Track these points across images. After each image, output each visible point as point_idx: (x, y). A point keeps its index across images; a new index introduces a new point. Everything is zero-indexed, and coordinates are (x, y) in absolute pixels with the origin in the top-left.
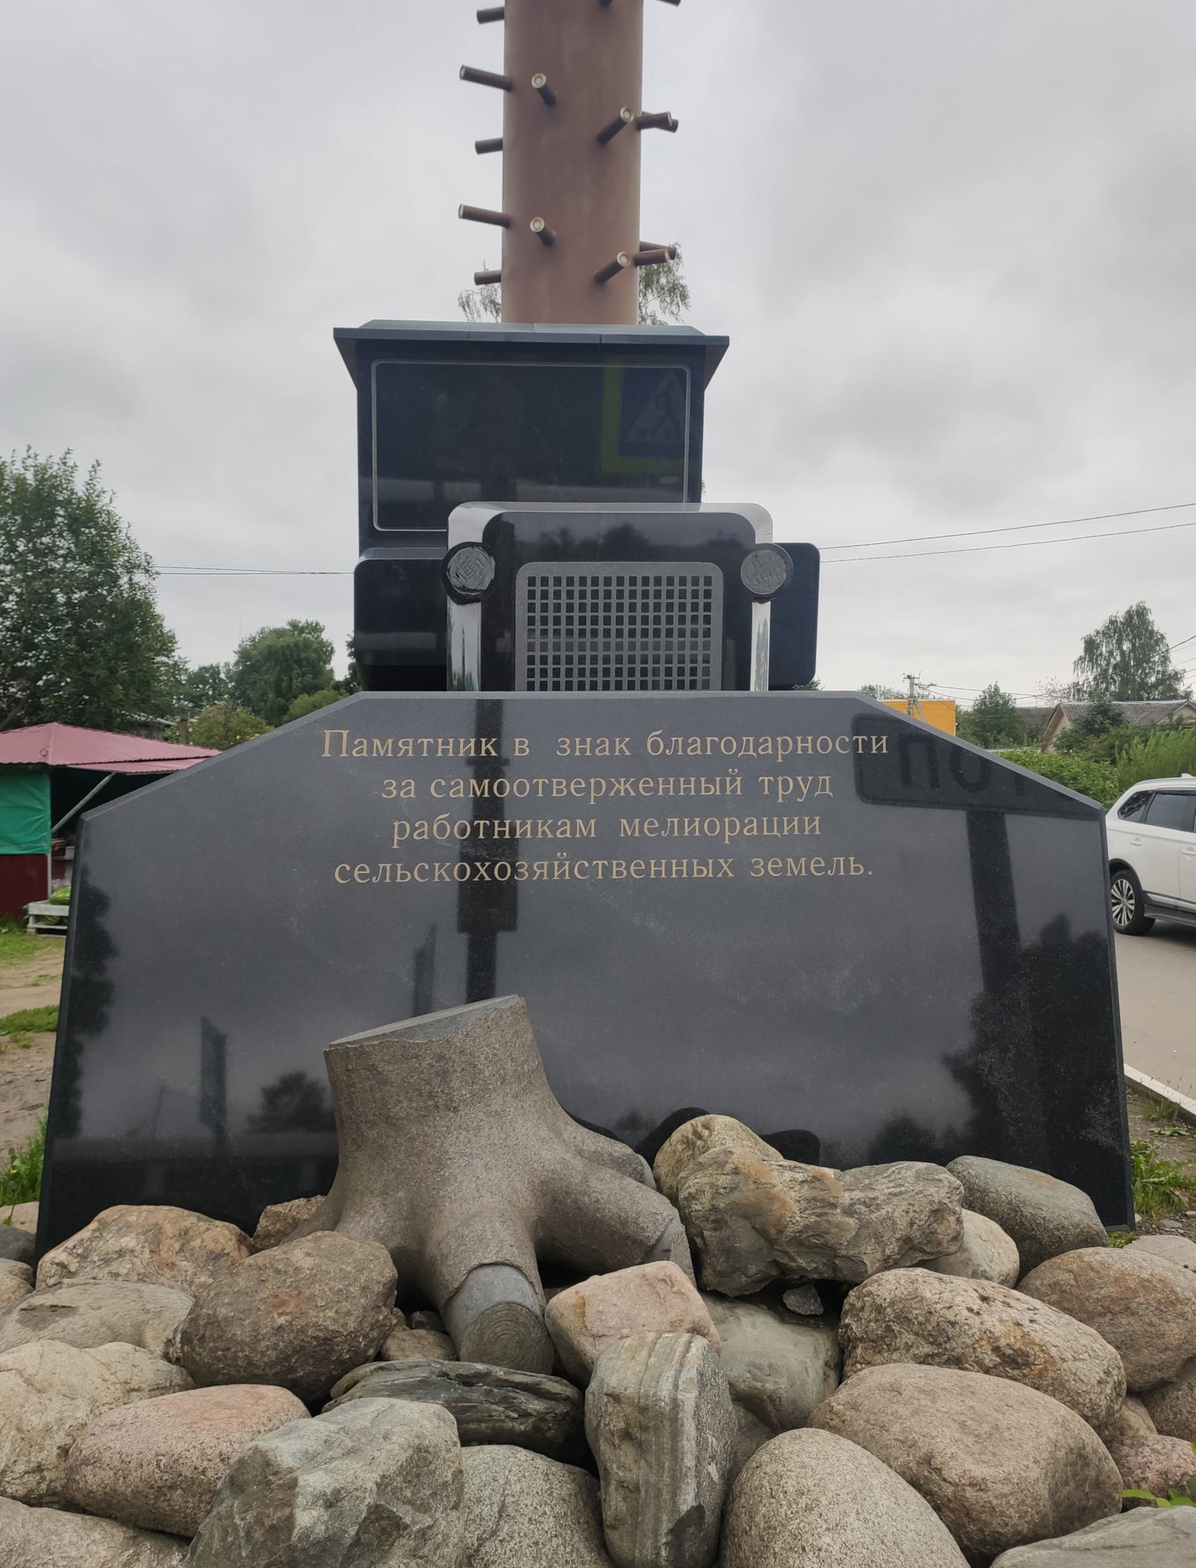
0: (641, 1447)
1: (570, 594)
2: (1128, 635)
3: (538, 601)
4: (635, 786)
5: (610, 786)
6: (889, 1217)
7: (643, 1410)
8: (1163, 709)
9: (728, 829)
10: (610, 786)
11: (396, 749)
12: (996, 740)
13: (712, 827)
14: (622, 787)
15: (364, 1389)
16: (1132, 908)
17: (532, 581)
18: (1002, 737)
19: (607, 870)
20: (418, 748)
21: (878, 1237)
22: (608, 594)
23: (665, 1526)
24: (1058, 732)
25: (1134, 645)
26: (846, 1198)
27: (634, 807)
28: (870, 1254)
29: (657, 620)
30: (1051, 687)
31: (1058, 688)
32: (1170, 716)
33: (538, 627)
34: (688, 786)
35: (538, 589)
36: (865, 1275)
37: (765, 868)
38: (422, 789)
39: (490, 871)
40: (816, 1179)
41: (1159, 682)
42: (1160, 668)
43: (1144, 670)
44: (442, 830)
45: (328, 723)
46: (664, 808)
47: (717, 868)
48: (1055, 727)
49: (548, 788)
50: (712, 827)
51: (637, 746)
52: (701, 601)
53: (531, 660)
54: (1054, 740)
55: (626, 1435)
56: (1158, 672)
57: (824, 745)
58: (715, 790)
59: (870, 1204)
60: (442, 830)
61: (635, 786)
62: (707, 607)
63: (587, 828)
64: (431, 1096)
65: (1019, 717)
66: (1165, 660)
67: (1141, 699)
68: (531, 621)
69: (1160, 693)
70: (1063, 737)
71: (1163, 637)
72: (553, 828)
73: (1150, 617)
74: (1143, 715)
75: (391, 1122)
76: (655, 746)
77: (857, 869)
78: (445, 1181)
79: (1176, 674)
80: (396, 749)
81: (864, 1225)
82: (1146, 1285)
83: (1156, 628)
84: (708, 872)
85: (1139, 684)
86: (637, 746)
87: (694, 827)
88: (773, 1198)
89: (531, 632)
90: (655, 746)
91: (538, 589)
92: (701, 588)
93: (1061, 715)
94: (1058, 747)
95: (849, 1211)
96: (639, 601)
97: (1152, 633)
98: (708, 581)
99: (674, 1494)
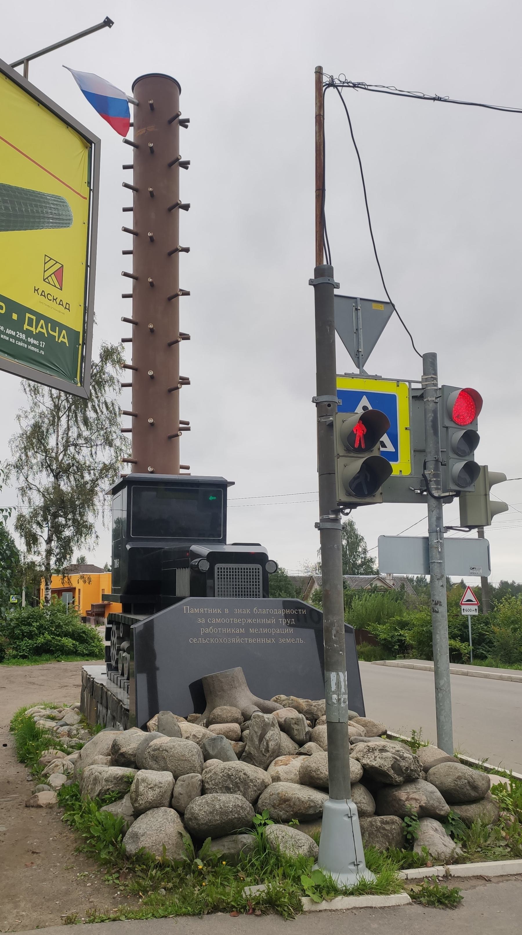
0: (298, 725)
1: (227, 572)
2: (344, 536)
3: (220, 574)
4: (252, 621)
5: (247, 621)
6: (322, 707)
7: (298, 719)
8: (366, 580)
9: (273, 631)
10: (247, 621)
11: (200, 611)
12: (279, 595)
13: (270, 631)
14: (249, 621)
15: (270, 703)
16: (385, 438)
17: (218, 569)
18: (283, 593)
19: (248, 641)
20: (204, 611)
21: (321, 711)
22: (236, 572)
23: (304, 733)
24: (313, 591)
25: (348, 542)
26: (314, 704)
27: (253, 626)
28: (320, 714)
29: (247, 578)
30: (306, 565)
31: (310, 565)
32: (371, 585)
33: (220, 580)
34: (263, 621)
35: (220, 570)
36: (319, 717)
37: (282, 641)
38: (206, 621)
39: (222, 640)
40: (307, 701)
41: (363, 564)
42: (363, 556)
43: (354, 557)
44: (211, 630)
45: (185, 604)
46: (259, 626)
47: (271, 641)
48: (311, 588)
49: (233, 621)
50: (270, 631)
51: (252, 611)
52: (257, 574)
53: (218, 588)
54: (311, 596)
55: (295, 723)
56: (362, 558)
57: (292, 611)
58: (269, 622)
59: (318, 705)
60: (211, 630)
61: (252, 621)
62: (259, 575)
63: (242, 631)
64: (231, 685)
65: (290, 581)
66: (365, 551)
67: (355, 574)
68: (218, 578)
69: (364, 570)
70: (316, 595)
71: (363, 539)
72: (235, 630)
73: (356, 527)
74: (355, 584)
75: (223, 690)
76: (255, 611)
77: (302, 642)
78: (237, 702)
79: (371, 559)
80: (200, 611)
81: (318, 709)
82: (369, 722)
83: (359, 533)
84: (269, 642)
85: (352, 564)
86: (252, 611)
87: (266, 631)
88: (300, 704)
89: (218, 581)
90: (255, 611)
91: (220, 570)
92: (257, 571)
93: (313, 582)
94: (313, 601)
95: (315, 706)
96: (243, 574)
97: (357, 536)
98: (259, 569)
99: (305, 729)
